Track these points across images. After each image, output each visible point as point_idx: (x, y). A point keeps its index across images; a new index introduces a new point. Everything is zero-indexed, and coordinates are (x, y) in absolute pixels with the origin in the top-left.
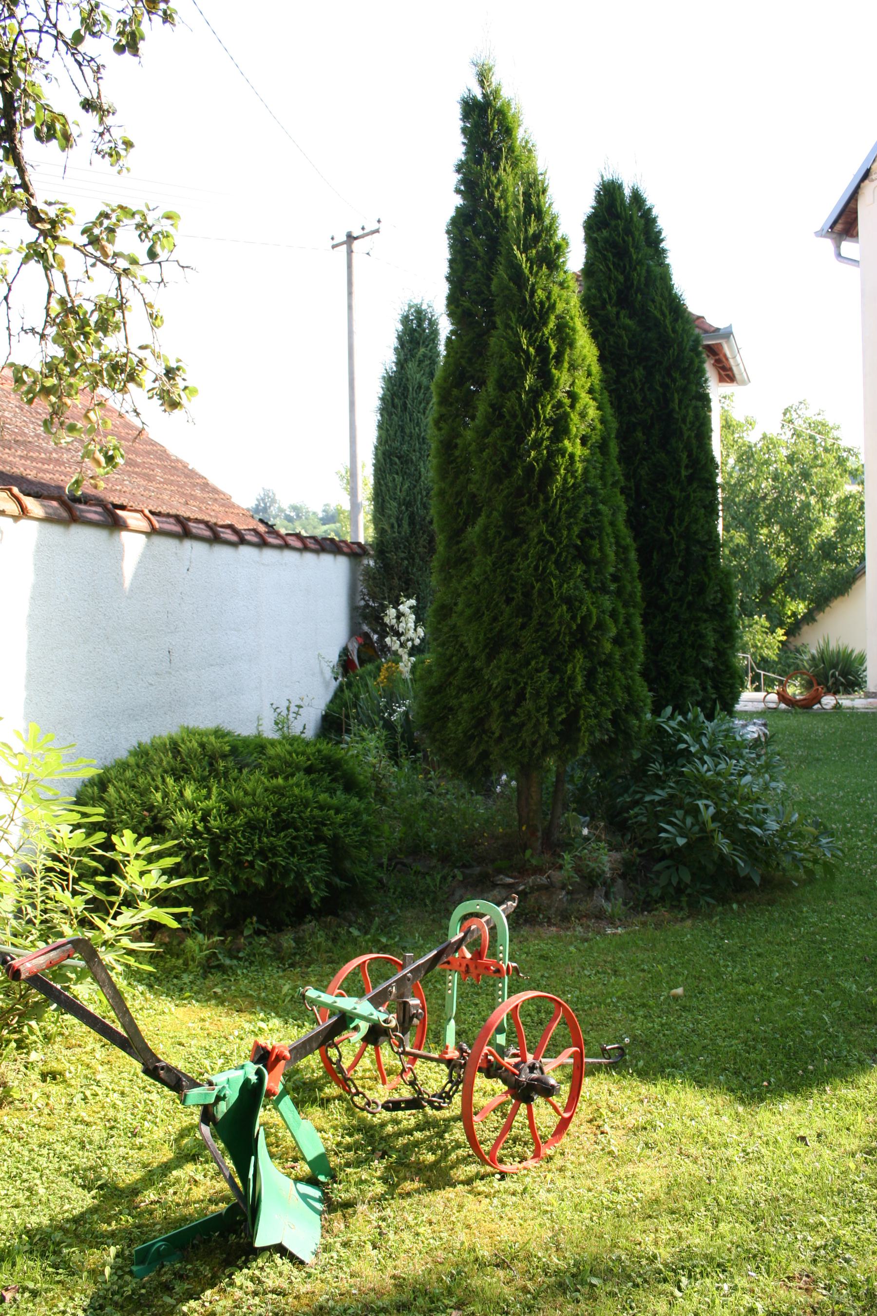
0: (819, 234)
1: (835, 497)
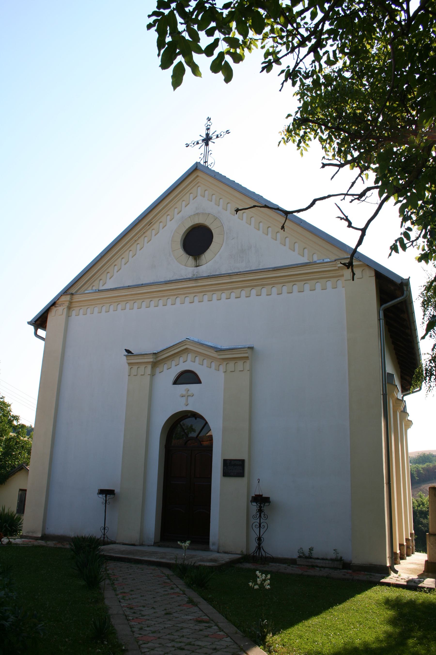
0: (29, 323)
1: (5, 437)
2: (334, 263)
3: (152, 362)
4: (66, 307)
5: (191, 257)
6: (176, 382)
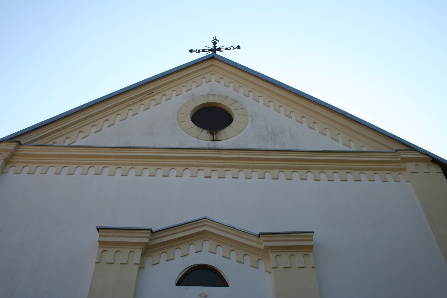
2: (395, 154)
3: (146, 244)
4: (3, 158)
5: (205, 131)
6: (181, 282)
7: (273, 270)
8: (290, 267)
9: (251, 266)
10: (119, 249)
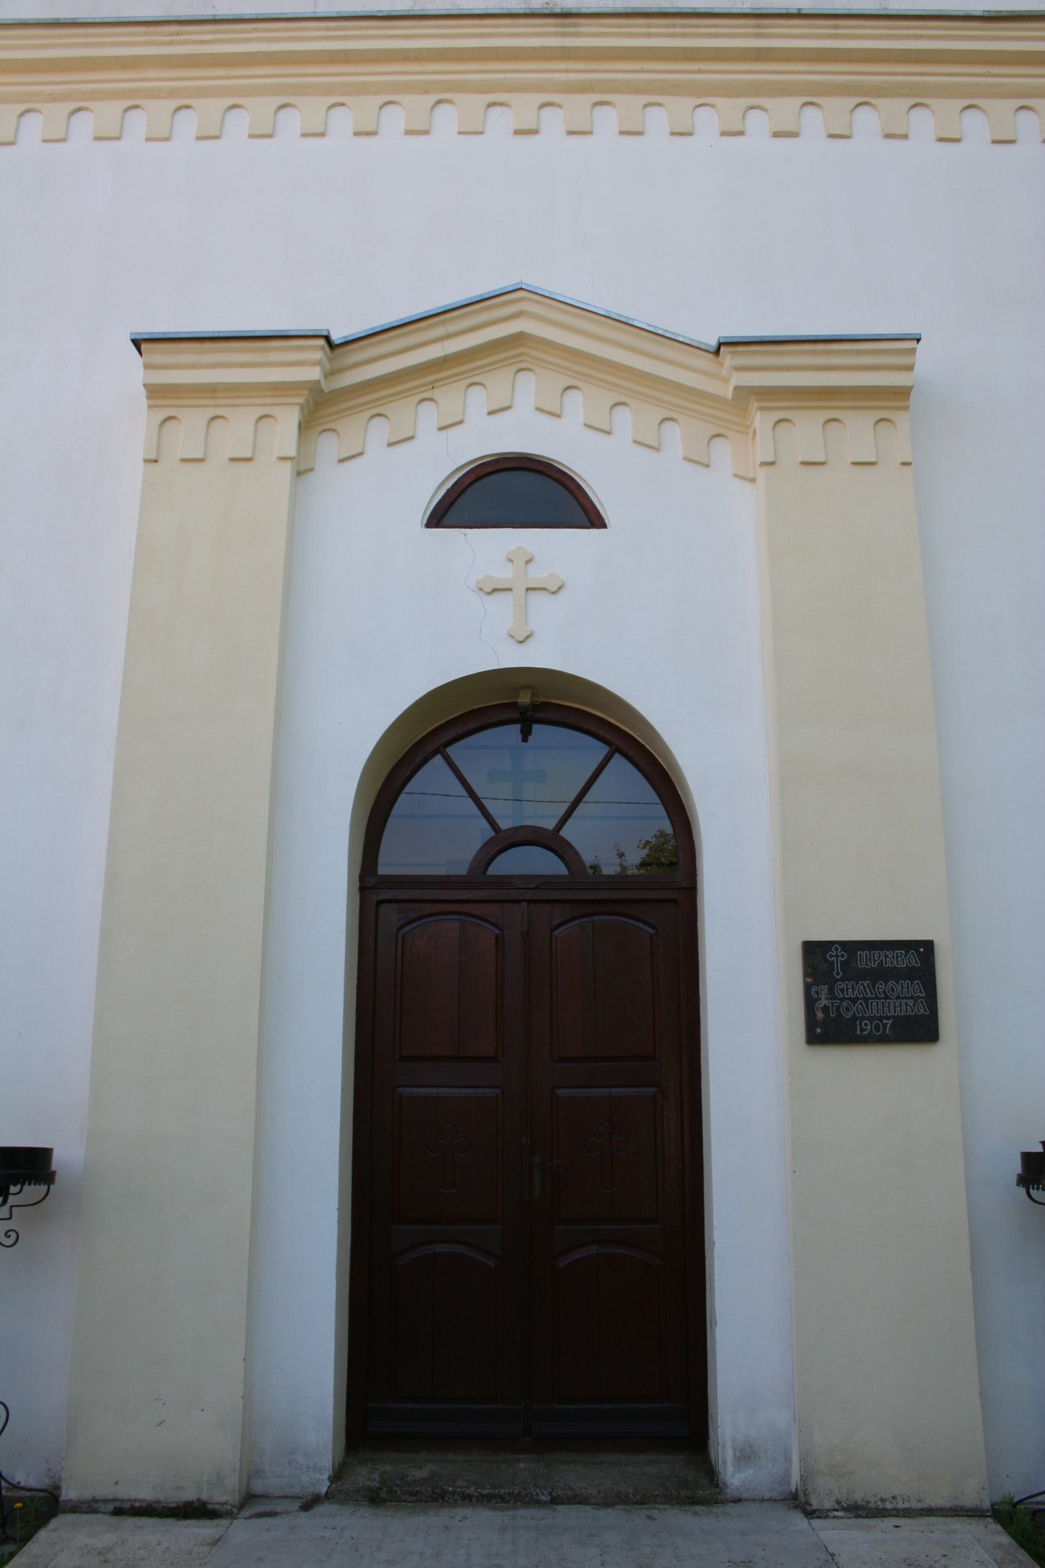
3: (313, 387)
6: (441, 516)
7: (761, 474)
8: (822, 463)
9: (686, 459)
10: (219, 412)
